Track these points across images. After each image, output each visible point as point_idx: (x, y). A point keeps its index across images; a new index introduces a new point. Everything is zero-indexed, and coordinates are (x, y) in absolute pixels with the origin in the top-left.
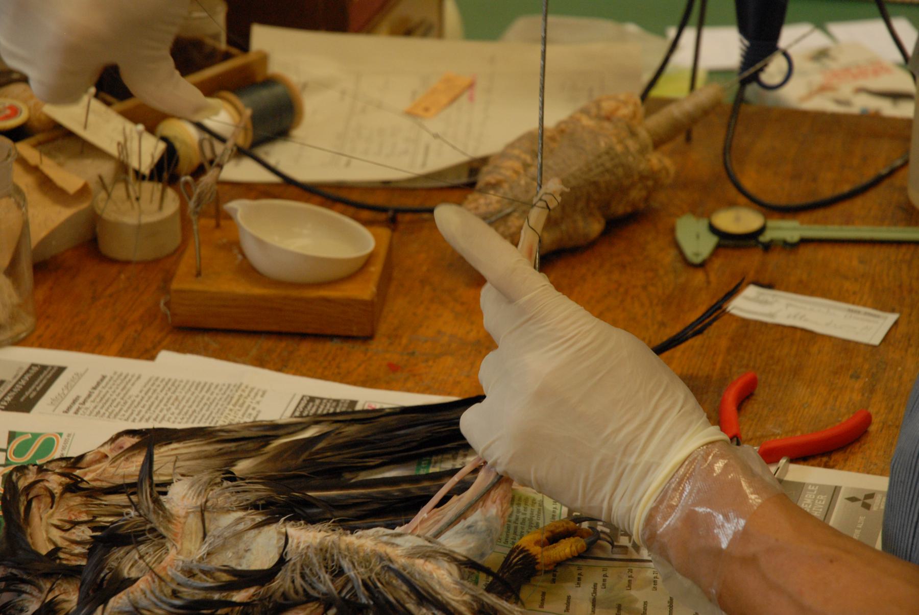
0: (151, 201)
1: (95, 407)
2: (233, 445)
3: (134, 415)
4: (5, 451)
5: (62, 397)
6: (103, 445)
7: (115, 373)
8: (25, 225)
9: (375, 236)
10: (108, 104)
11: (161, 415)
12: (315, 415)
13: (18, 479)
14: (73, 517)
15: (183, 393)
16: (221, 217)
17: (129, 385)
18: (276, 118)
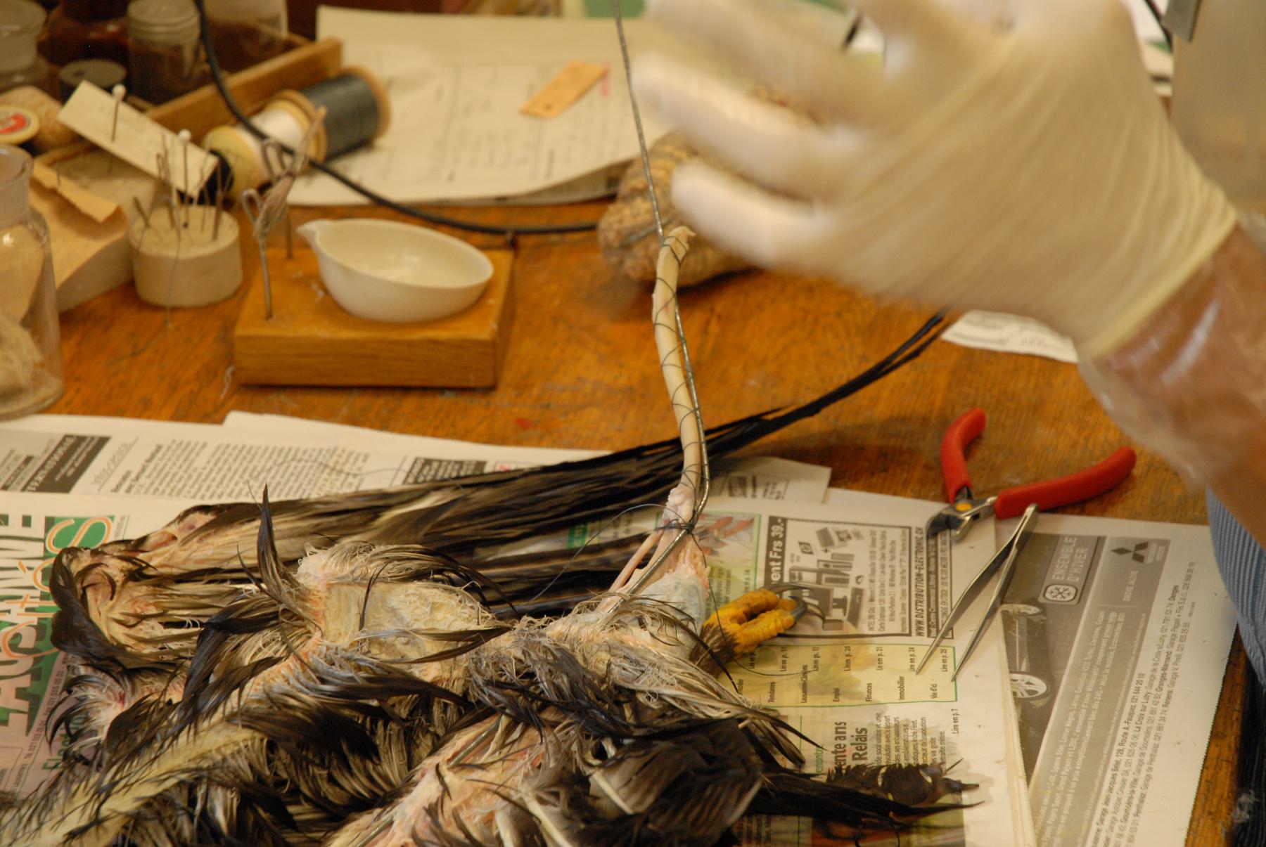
0: (202, 229)
1: (152, 483)
2: (333, 519)
3: (203, 491)
4: (43, 540)
5: (108, 473)
6: (169, 525)
7: (174, 442)
8: (47, 262)
9: (494, 261)
10: (141, 110)
11: (237, 489)
12: (433, 480)
13: (71, 561)
14: (139, 611)
15: (263, 462)
16: (296, 247)
17: (193, 455)
18: (356, 123)
